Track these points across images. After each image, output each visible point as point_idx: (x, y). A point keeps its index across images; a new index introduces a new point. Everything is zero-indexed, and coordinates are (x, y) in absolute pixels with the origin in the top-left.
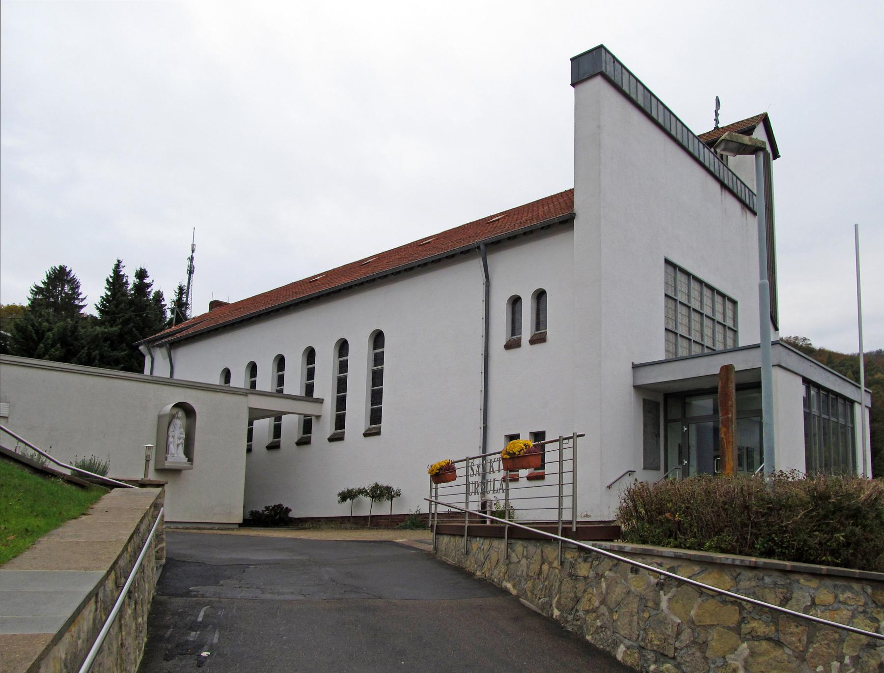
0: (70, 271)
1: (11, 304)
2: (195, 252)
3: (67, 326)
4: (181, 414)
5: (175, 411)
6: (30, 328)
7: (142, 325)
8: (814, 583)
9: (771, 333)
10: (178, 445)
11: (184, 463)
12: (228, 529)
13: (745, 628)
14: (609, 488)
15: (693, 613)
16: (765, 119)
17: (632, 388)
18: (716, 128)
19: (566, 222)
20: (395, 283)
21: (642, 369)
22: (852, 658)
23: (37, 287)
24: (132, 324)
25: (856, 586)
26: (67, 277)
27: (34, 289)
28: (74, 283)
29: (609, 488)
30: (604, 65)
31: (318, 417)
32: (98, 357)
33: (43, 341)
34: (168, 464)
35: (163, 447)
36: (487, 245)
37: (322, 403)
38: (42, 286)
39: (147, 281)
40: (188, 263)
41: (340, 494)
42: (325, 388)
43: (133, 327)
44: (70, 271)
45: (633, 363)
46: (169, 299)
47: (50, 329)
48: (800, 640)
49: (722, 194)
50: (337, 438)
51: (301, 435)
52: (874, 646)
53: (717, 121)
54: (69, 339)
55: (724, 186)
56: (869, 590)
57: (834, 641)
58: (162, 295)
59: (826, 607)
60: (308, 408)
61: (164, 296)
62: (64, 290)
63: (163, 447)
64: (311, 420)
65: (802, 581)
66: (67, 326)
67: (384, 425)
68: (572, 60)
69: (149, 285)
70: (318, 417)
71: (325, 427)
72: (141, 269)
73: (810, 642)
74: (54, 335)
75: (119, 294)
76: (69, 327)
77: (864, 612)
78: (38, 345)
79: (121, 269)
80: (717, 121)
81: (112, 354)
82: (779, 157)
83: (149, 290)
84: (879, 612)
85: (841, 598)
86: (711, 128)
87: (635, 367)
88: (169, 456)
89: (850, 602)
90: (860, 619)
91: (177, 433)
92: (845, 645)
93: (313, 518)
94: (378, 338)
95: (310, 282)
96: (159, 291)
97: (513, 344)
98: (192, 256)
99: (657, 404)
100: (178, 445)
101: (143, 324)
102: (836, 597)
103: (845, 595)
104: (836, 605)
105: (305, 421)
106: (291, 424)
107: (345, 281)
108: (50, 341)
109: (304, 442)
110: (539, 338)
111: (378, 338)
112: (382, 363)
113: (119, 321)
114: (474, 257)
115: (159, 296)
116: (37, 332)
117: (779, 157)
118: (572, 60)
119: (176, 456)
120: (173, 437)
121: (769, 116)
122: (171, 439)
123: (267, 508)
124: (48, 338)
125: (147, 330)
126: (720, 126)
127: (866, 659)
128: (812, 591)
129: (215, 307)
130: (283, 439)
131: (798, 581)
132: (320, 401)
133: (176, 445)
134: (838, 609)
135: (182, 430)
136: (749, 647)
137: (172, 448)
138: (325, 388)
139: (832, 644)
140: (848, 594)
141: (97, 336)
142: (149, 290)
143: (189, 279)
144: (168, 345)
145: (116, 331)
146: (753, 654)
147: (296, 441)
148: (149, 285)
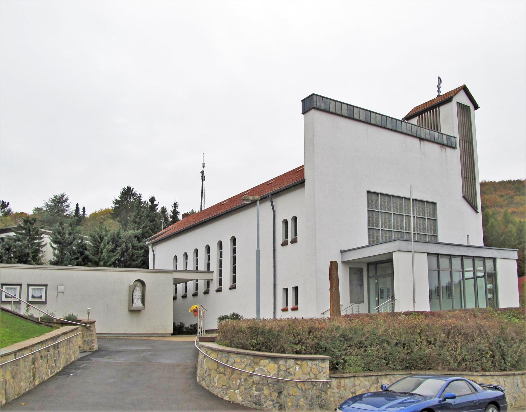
0: (133, 189)
1: (106, 208)
2: (200, 178)
3: (114, 232)
4: (139, 284)
5: (137, 283)
6: (96, 236)
7: (153, 227)
8: (235, 356)
9: (216, 278)
10: (138, 299)
11: (141, 307)
12: (150, 337)
13: (218, 370)
14: (323, 314)
15: (209, 365)
16: (465, 89)
17: (341, 263)
18: (439, 96)
19: (301, 184)
20: (243, 211)
21: (347, 253)
22: (244, 379)
23: (116, 200)
24: (148, 227)
25: (248, 357)
26: (131, 193)
27: (114, 201)
28: (135, 195)
29: (323, 314)
30: (315, 103)
31: (212, 280)
32: (131, 247)
33: (103, 242)
34: (133, 308)
35: (131, 301)
36: (272, 195)
37: (213, 273)
38: (119, 199)
39: (155, 203)
40: (201, 175)
41: (218, 318)
42: (214, 267)
43: (149, 228)
44: (133, 189)
45: (341, 250)
46: (170, 210)
47: (106, 235)
48: (229, 374)
49: (420, 144)
50: (233, 288)
51: (232, 284)
52: (252, 376)
53: (439, 91)
54: (116, 239)
55: (421, 139)
56: (252, 358)
57: (239, 374)
58: (165, 209)
59: (238, 363)
60: (208, 276)
61: (167, 209)
62: (130, 200)
63: (131, 301)
64: (209, 281)
65: (232, 355)
66: (114, 232)
67: (237, 283)
68: (302, 101)
69: (157, 205)
70: (212, 280)
71: (214, 286)
72: (152, 197)
73: (232, 374)
74: (108, 238)
75: (141, 212)
76: (116, 233)
77: (250, 365)
78: (101, 244)
79: (141, 198)
80: (439, 91)
81: (138, 244)
82: (479, 107)
83: (157, 208)
84: (255, 365)
85: (243, 360)
86: (435, 95)
87: (342, 252)
88: (133, 304)
89: (245, 362)
90: (248, 367)
91: (138, 293)
92: (242, 375)
93: (211, 330)
94: (234, 240)
95: (221, 205)
96: (164, 207)
97: (284, 244)
98: (203, 170)
99: (361, 270)
100: (138, 299)
101: (154, 226)
102: (241, 360)
103: (244, 360)
104: (241, 363)
105: (207, 281)
106: (202, 284)
107: (220, 212)
108: (106, 241)
109: (207, 292)
110: (294, 241)
111: (234, 240)
112: (222, 257)
113: (141, 226)
114: (267, 201)
115: (164, 210)
116: (100, 237)
117: (479, 107)
118: (302, 101)
119: (137, 303)
120: (136, 295)
121: (467, 86)
122: (134, 297)
123: (191, 326)
124: (105, 240)
125: (156, 229)
126: (441, 94)
127: (249, 380)
128: (234, 358)
129: (185, 217)
130: (199, 291)
131: (231, 355)
132: (212, 272)
133: (137, 299)
134: (242, 364)
135: (140, 292)
136: (219, 376)
137: (135, 301)
138: (214, 267)
139: (238, 375)
140: (245, 359)
141: (130, 236)
142: (157, 208)
143: (202, 184)
144: (151, 244)
145: (139, 232)
146: (219, 378)
147: (203, 292)
148: (157, 205)
